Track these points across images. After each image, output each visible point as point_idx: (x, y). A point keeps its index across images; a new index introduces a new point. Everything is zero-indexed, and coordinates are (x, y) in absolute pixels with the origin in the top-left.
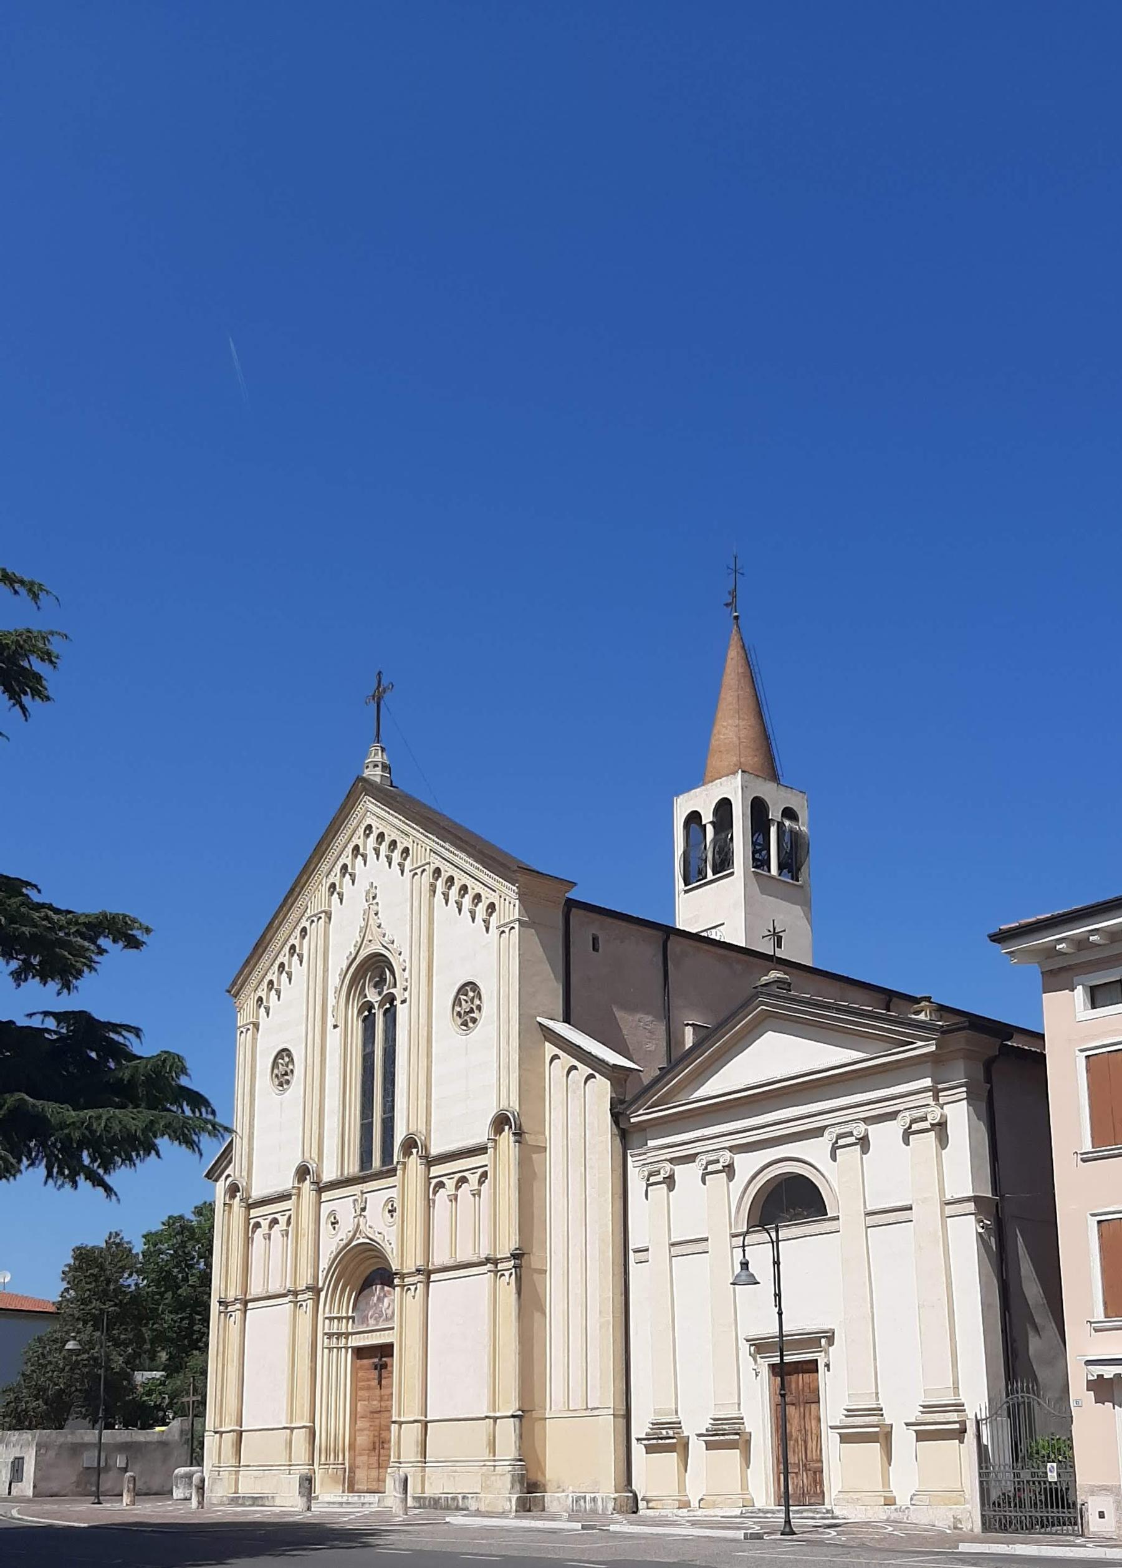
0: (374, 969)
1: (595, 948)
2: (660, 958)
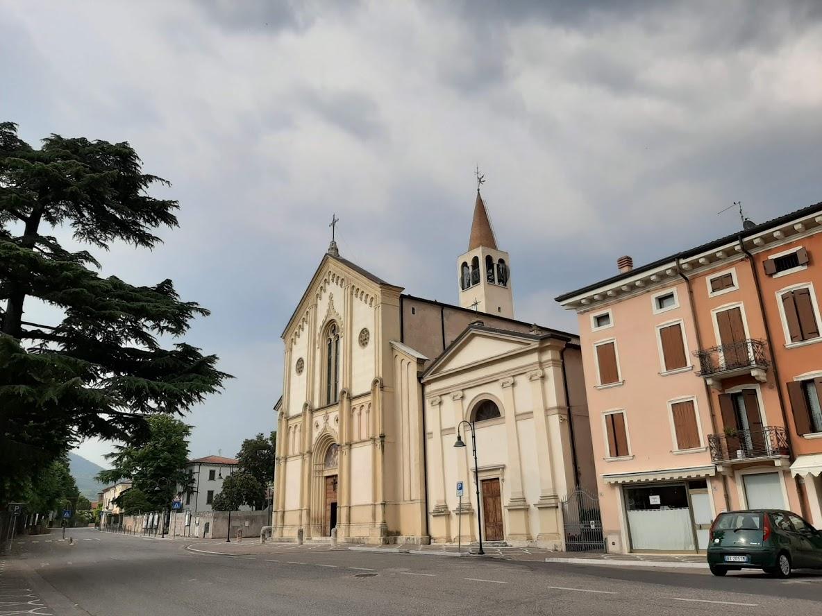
0: (331, 327)
1: (413, 313)
2: (440, 315)
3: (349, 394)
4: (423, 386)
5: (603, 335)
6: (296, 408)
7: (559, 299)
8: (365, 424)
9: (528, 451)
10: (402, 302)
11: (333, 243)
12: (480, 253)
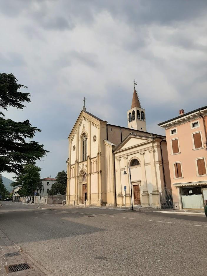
0: (84, 135)
1: (111, 130)
3: (90, 157)
4: (114, 155)
5: (174, 136)
6: (73, 162)
7: (159, 125)
8: (96, 167)
9: (149, 175)
10: (107, 128)
11: (84, 107)
12: (135, 109)
